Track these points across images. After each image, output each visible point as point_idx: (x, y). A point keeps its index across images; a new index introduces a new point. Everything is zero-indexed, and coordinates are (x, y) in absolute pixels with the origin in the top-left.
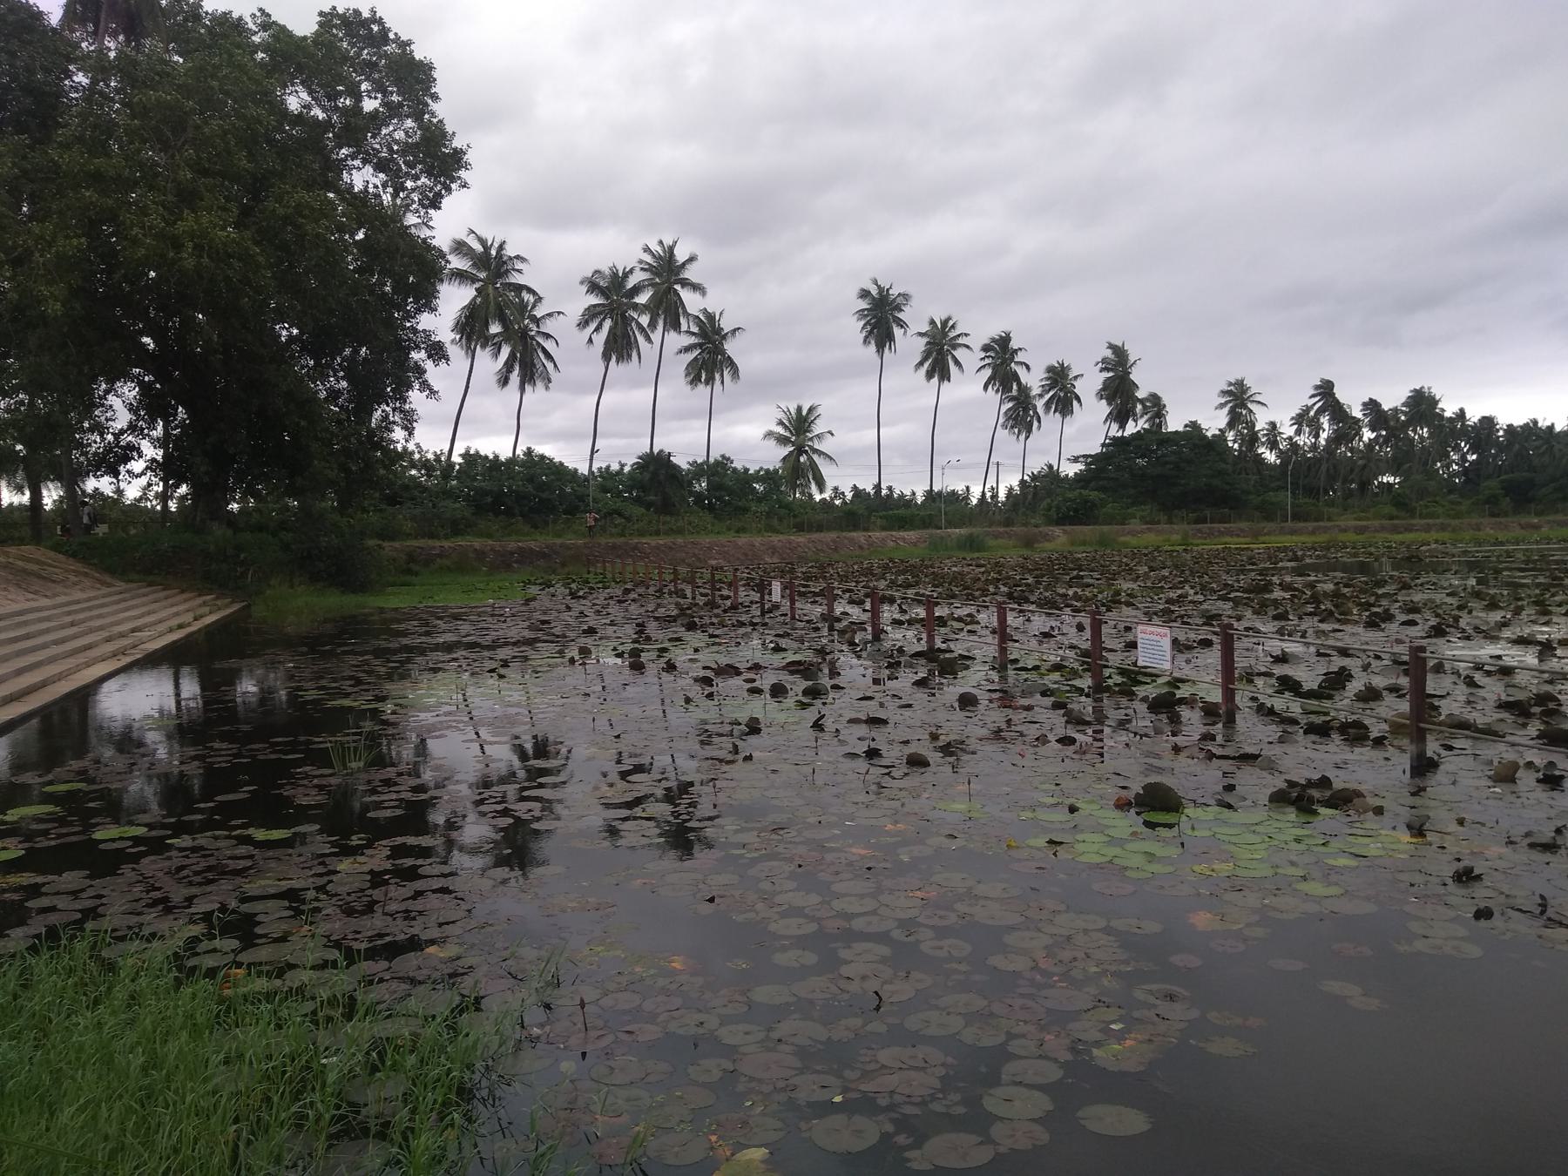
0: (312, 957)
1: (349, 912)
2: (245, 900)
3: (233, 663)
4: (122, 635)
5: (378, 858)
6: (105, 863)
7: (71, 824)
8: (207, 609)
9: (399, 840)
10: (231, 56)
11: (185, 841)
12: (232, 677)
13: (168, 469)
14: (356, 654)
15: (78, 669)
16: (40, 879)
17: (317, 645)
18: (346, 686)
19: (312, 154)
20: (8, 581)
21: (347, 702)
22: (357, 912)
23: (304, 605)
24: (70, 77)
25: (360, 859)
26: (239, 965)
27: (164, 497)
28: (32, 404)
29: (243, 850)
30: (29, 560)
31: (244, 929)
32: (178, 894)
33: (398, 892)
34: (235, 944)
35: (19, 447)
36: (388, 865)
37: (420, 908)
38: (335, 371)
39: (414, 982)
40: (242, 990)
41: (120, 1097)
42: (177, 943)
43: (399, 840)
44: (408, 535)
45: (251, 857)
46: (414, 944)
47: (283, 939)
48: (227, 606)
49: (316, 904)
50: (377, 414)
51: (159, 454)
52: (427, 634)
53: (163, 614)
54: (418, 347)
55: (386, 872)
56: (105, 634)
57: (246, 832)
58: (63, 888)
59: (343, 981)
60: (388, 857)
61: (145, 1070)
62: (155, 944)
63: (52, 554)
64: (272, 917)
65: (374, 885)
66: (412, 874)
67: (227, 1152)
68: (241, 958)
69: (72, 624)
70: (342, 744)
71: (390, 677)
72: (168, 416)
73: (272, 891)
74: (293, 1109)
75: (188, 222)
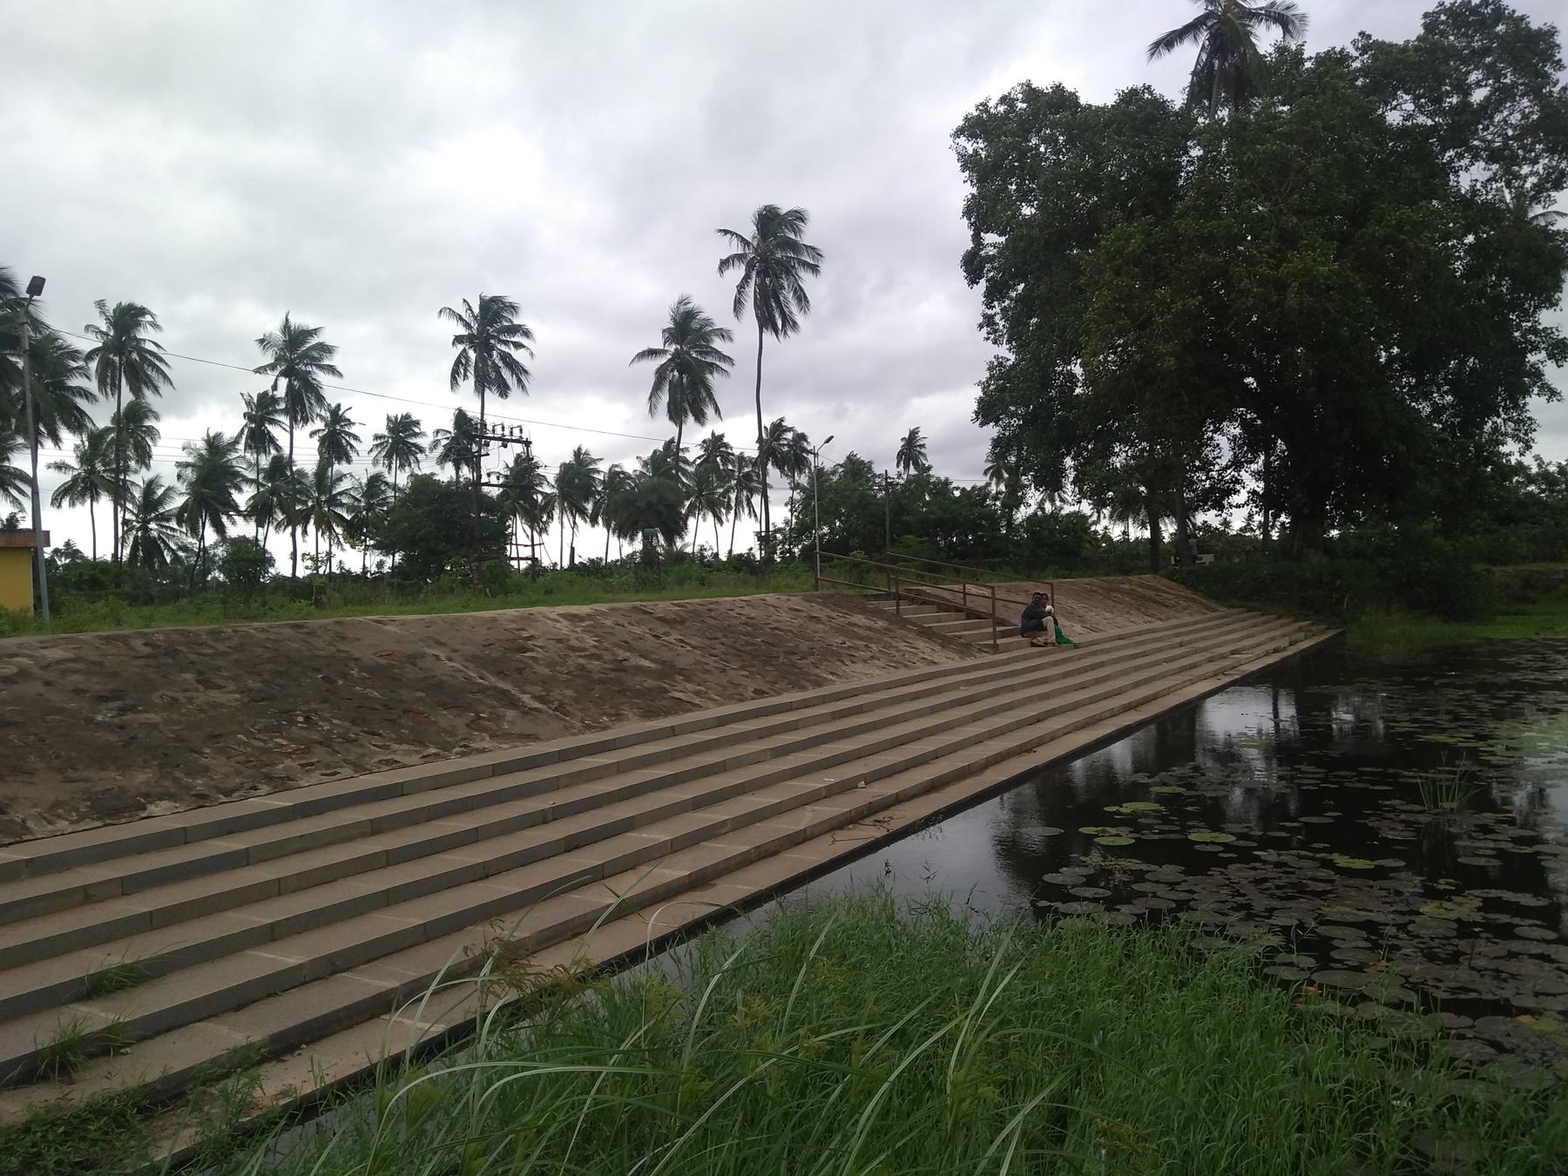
0: (1384, 994)
1: (1431, 957)
2: (1324, 922)
3: (1324, 689)
4: (1223, 657)
5: (1467, 907)
6: (1198, 863)
7: (1171, 823)
8: (1302, 635)
9: (1494, 893)
10: (1335, 90)
11: (1270, 855)
12: (1326, 704)
13: (1267, 501)
14: (1455, 687)
15: (1184, 685)
16: (1144, 867)
17: (1415, 676)
18: (1444, 720)
19: (1420, 160)
20: (1131, 606)
21: (1442, 738)
22: (1440, 959)
23: (1399, 633)
24: (1187, 152)
25: (1446, 904)
26: (1311, 983)
27: (1265, 526)
28: (1152, 450)
29: (1324, 873)
30: (1148, 587)
31: (1321, 950)
32: (1260, 903)
33: (1486, 949)
34: (1311, 962)
35: (1142, 489)
36: (1478, 917)
37: (1513, 970)
38: (1439, 387)
39: (1500, 1048)
40: (1312, 1007)
41: (1196, 1073)
42: (1255, 950)
43: (1494, 893)
44: (1524, 559)
45: (1331, 882)
46: (1504, 1009)
47: (1359, 969)
48: (1322, 632)
49: (1395, 942)
50: (1488, 427)
51: (1260, 487)
52: (1542, 669)
53: (1261, 638)
54: (1535, 348)
55: (1476, 924)
56: (1209, 655)
57: (1329, 857)
58: (1162, 877)
59: (1419, 1026)
60: (1479, 909)
61: (1220, 1055)
62: (1238, 946)
63: (1166, 581)
64: (1349, 945)
65: (1461, 936)
66: (1507, 932)
67: (1289, 1158)
68: (1315, 977)
69: (1181, 645)
70: (1434, 781)
71: (1498, 715)
72: (1269, 449)
73: (1350, 919)
74: (1355, 1138)
75: (1295, 262)
